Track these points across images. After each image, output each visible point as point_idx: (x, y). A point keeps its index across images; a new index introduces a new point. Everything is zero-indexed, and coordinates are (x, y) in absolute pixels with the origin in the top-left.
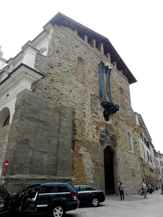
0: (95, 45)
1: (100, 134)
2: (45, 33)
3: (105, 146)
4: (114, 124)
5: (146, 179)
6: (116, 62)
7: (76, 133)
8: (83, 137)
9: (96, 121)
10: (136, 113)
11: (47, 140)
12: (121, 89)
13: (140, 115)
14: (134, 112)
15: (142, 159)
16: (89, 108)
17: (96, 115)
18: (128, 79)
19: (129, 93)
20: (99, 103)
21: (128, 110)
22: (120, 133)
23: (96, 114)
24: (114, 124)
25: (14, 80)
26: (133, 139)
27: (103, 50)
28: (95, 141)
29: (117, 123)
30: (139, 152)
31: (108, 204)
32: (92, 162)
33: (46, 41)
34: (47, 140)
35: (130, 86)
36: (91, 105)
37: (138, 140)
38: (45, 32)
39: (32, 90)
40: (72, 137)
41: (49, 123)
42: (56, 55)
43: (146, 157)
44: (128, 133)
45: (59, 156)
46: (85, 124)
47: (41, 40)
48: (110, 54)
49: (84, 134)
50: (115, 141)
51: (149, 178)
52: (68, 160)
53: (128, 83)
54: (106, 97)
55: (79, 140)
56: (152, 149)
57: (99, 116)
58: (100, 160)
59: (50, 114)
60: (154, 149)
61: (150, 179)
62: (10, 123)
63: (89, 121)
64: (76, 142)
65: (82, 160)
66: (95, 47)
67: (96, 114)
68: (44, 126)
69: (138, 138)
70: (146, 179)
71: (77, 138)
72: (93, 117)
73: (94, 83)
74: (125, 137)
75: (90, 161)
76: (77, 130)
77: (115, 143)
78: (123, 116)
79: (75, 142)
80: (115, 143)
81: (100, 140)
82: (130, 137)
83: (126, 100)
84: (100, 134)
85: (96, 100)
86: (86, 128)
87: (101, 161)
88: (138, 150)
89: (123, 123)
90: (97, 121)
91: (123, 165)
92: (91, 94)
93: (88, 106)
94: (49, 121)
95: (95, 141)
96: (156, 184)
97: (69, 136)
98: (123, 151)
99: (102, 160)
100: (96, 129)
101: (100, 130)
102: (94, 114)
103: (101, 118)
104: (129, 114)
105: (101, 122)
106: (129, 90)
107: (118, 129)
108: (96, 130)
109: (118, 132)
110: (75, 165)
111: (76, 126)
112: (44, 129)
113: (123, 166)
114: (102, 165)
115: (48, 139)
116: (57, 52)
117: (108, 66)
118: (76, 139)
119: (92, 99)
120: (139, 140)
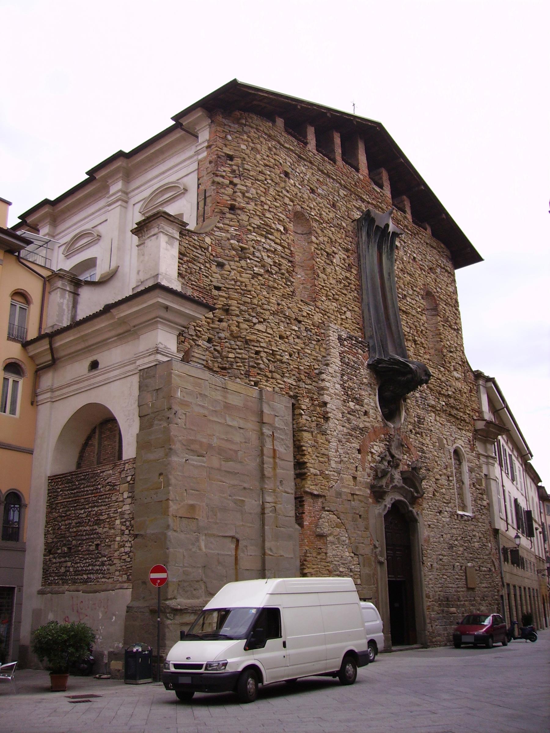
0: (340, 151)
1: (371, 468)
2: (179, 134)
3: (388, 501)
4: (410, 427)
5: (509, 595)
6: (409, 197)
7: (305, 474)
8: (324, 482)
9: (358, 426)
10: (478, 375)
11: (235, 503)
12: (428, 295)
13: (492, 380)
14: (474, 369)
15: (496, 532)
16: (338, 386)
17: (357, 407)
18: (452, 252)
19: (456, 304)
20: (366, 364)
21: (455, 370)
22: (432, 452)
23: (359, 401)
24: (410, 427)
25: (123, 321)
26: (471, 470)
27: (365, 162)
28: (357, 493)
29: (419, 422)
30: (488, 510)
31: (66, 698)
32: (353, 555)
33: (185, 161)
34: (235, 502)
35: (459, 273)
36: (343, 375)
37: (485, 471)
38: (179, 130)
39: (181, 355)
40: (297, 487)
41: (236, 452)
42: (228, 222)
43: (510, 521)
44: (456, 452)
45: (267, 545)
46: (329, 442)
47: (161, 151)
48: (389, 171)
49: (327, 472)
50: (417, 484)
51: (518, 594)
52: (290, 556)
53: (449, 266)
54: (386, 341)
55: (316, 492)
56: (533, 486)
57: (366, 407)
58: (375, 547)
59: (235, 424)
60: (540, 484)
61: (521, 595)
62: (125, 457)
63: (340, 428)
64: (308, 501)
65: (326, 553)
66: (339, 158)
67: (359, 401)
68: (223, 462)
69: (487, 464)
70: (509, 595)
71: (310, 486)
72: (349, 413)
73: (345, 295)
74: (446, 468)
75: (347, 554)
76: (306, 463)
77: (417, 492)
78: (440, 393)
79: (303, 501)
80: (417, 492)
81: (372, 487)
82: (460, 464)
83: (448, 334)
84: (371, 468)
85: (355, 355)
86: (332, 453)
87: (378, 550)
88: (485, 503)
89: (438, 418)
90: (361, 426)
91: (441, 557)
92: (340, 338)
93: (334, 380)
94: (234, 447)
95: (360, 490)
96: (542, 610)
97: (290, 486)
98: (440, 512)
99: (379, 549)
100: (359, 451)
101: (372, 453)
102: (351, 404)
103: (371, 412)
104: (458, 385)
105: (373, 426)
106: (455, 292)
107: (423, 444)
108: (359, 456)
109: (423, 452)
110: (308, 568)
111: (306, 452)
112: (226, 471)
113: (441, 560)
114: (381, 563)
115: (236, 500)
116: (232, 208)
117: (387, 226)
118: (307, 493)
119: (343, 352)
120: (488, 470)
